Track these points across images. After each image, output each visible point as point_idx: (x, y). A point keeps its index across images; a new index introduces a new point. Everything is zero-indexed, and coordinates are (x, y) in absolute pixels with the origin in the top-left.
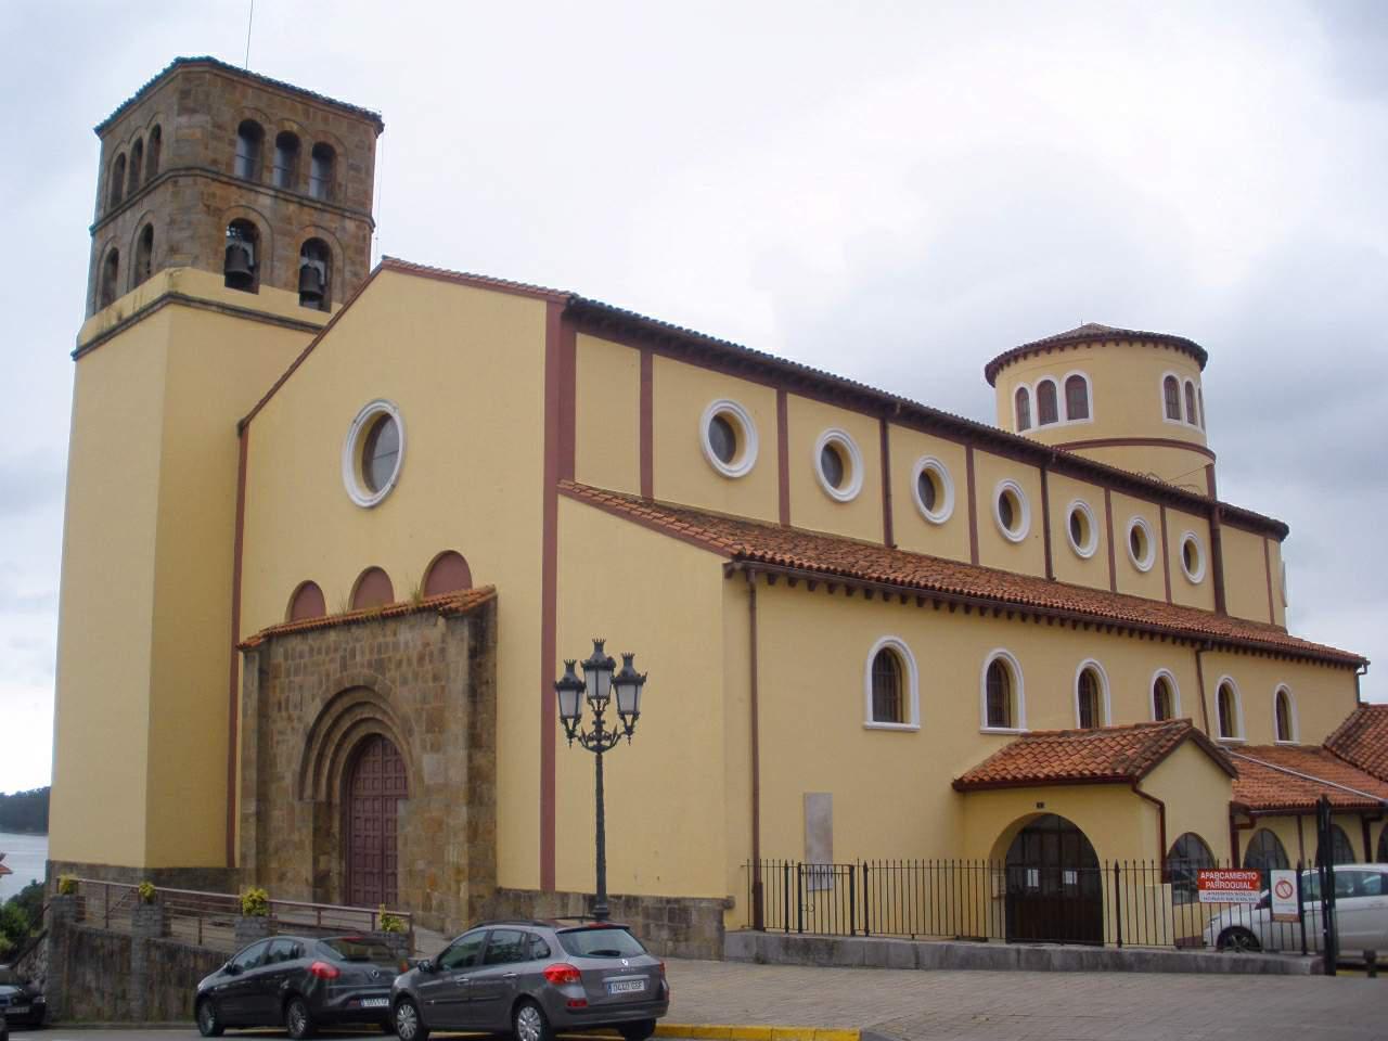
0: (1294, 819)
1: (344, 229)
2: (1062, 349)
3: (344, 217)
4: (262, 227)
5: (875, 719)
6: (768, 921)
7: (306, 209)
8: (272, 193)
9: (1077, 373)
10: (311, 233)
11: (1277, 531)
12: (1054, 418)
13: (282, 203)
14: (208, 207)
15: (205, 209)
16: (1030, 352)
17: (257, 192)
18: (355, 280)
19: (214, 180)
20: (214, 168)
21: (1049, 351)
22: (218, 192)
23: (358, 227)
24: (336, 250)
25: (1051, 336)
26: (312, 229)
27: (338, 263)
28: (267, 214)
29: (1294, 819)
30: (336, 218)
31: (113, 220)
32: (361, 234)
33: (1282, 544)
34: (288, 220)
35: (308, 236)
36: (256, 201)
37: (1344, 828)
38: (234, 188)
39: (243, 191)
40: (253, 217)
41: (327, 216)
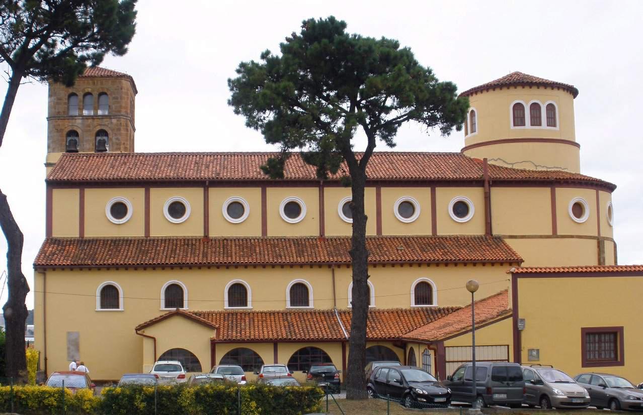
0: (271, 347)
1: (112, 123)
2: (494, 90)
3: (111, 118)
4: (79, 131)
5: (229, 306)
6: (477, 386)
7: (96, 120)
8: (81, 118)
9: (517, 101)
10: (98, 128)
11: (610, 188)
12: (523, 124)
13: (86, 120)
14: (57, 129)
15: (56, 131)
16: (484, 89)
17: (76, 119)
18: (117, 141)
19: (58, 119)
20: (59, 116)
21: (487, 90)
22: (60, 123)
23: (118, 121)
24: (109, 132)
25: (490, 81)
26: (99, 127)
27: (110, 136)
28: (80, 126)
29: (272, 346)
30: (108, 120)
31: (87, 119)
32: (119, 123)
33: (612, 193)
34: (89, 126)
35: (98, 129)
36: (75, 122)
37: (326, 350)
38: (66, 120)
39: (70, 120)
40: (75, 128)
41: (105, 120)
